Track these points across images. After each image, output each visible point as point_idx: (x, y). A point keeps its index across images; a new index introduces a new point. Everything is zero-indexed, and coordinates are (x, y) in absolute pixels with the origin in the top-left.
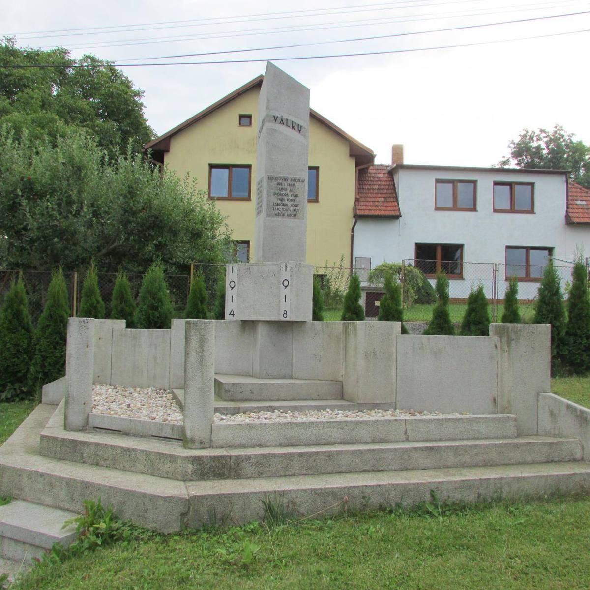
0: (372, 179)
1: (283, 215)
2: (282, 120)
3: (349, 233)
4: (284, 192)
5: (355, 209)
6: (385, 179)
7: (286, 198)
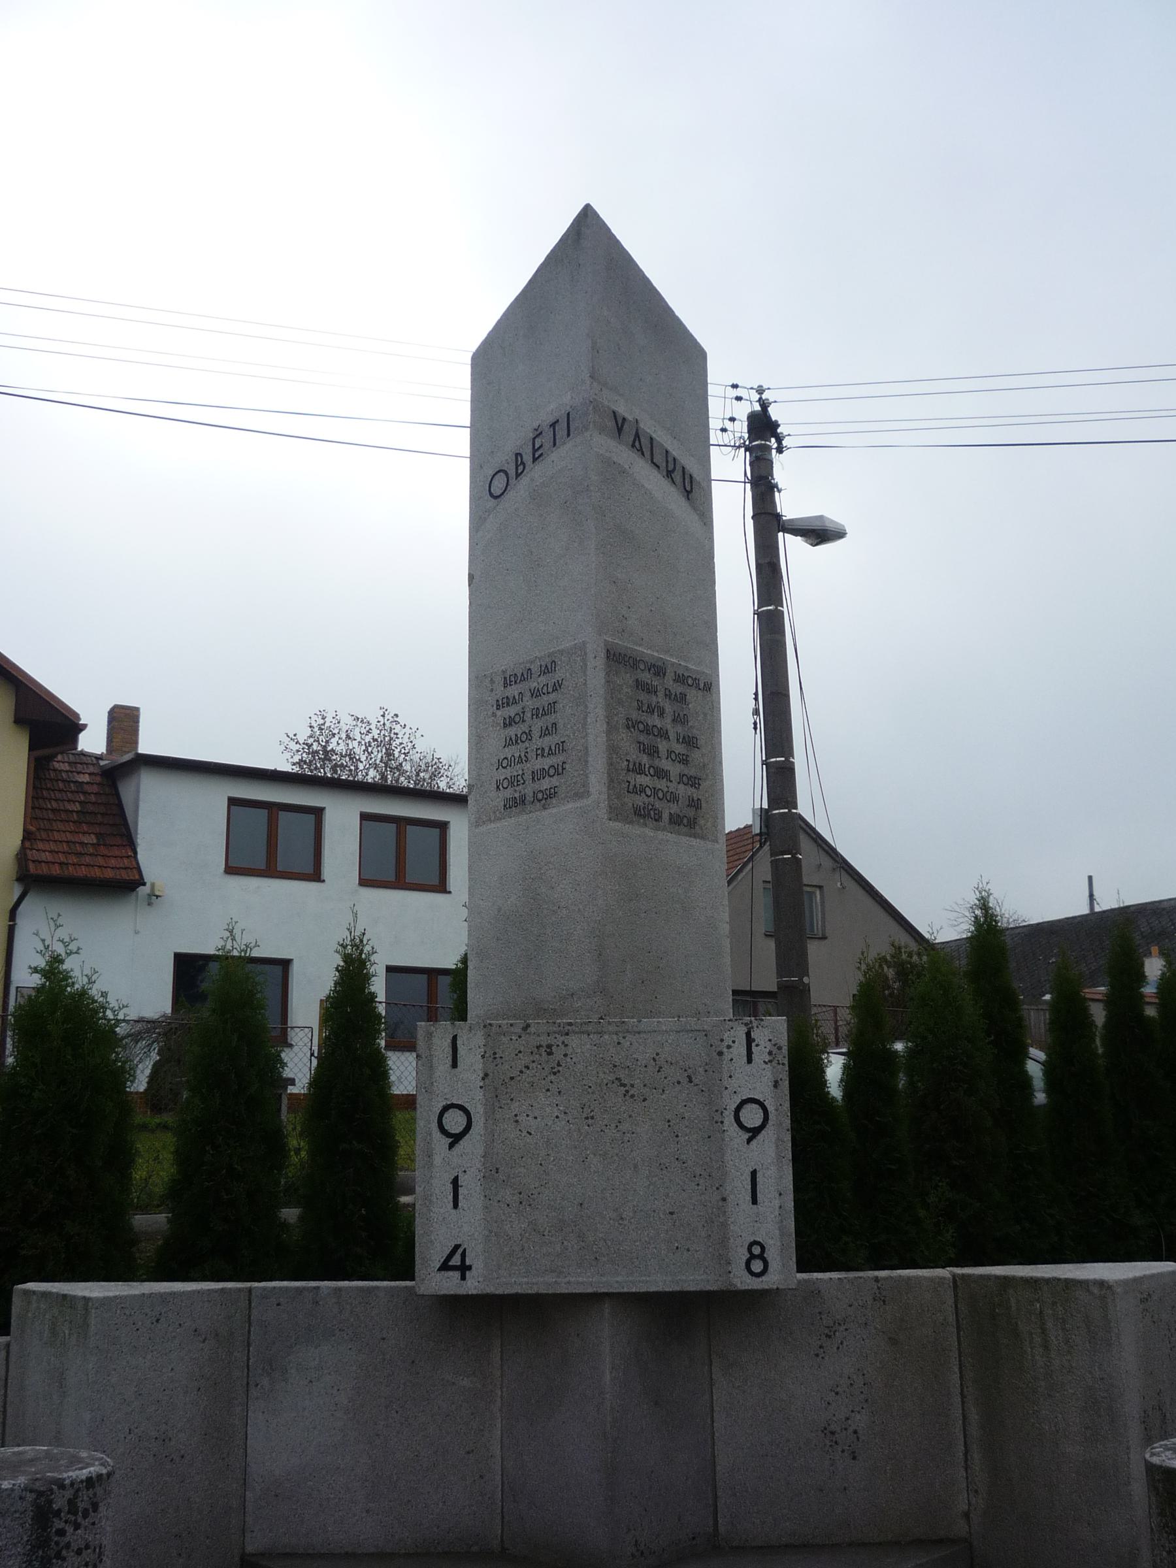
0: (61, 785)
1: (658, 819)
2: (637, 436)
4: (654, 720)
5: (22, 858)
6: (95, 789)
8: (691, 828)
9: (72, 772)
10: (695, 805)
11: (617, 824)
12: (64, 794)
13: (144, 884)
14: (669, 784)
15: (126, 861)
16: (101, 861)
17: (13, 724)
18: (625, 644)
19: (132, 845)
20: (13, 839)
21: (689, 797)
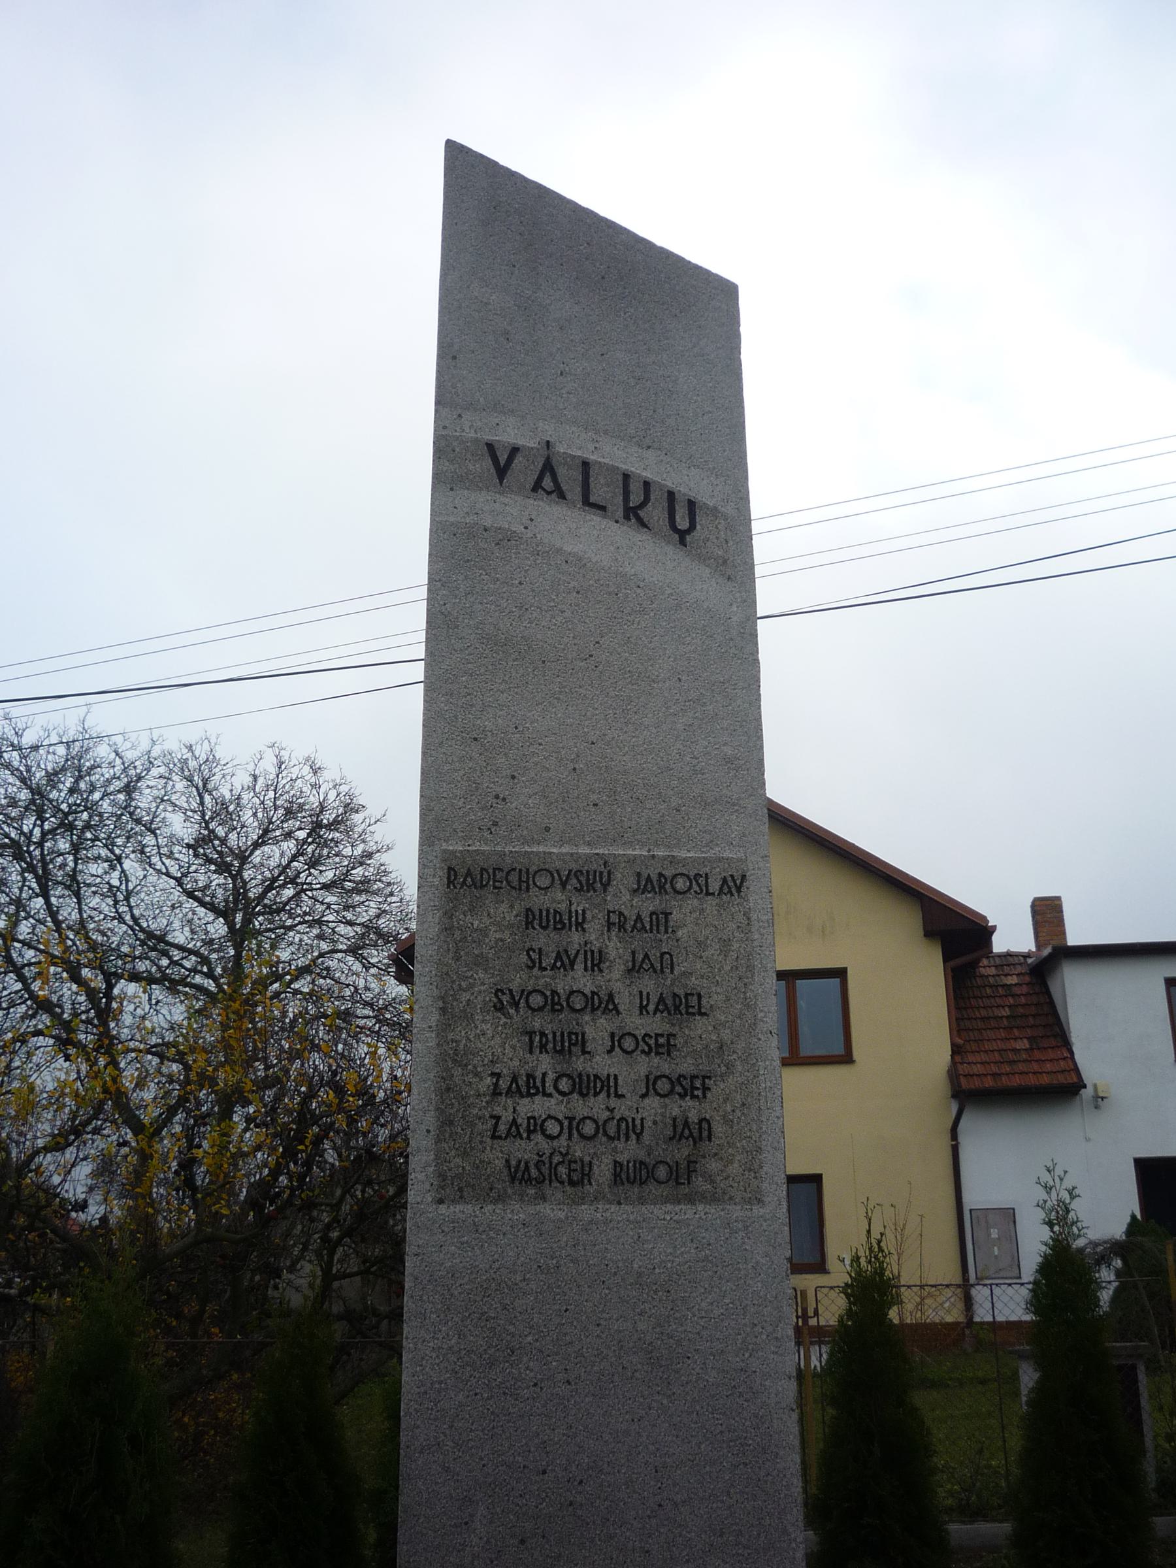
0: (989, 991)
1: (580, 1176)
2: (548, 467)
3: (945, 1142)
4: (582, 980)
5: (953, 1074)
6: (1025, 989)
7: (597, 1029)
8: (678, 1183)
9: (998, 975)
10: (691, 1135)
11: (459, 1207)
12: (992, 1000)
13: (1085, 1086)
14: (613, 1102)
15: (1062, 1063)
16: (1035, 1067)
17: (924, 938)
18: (499, 848)
19: (1066, 1044)
20: (943, 1055)
21: (674, 1119)
